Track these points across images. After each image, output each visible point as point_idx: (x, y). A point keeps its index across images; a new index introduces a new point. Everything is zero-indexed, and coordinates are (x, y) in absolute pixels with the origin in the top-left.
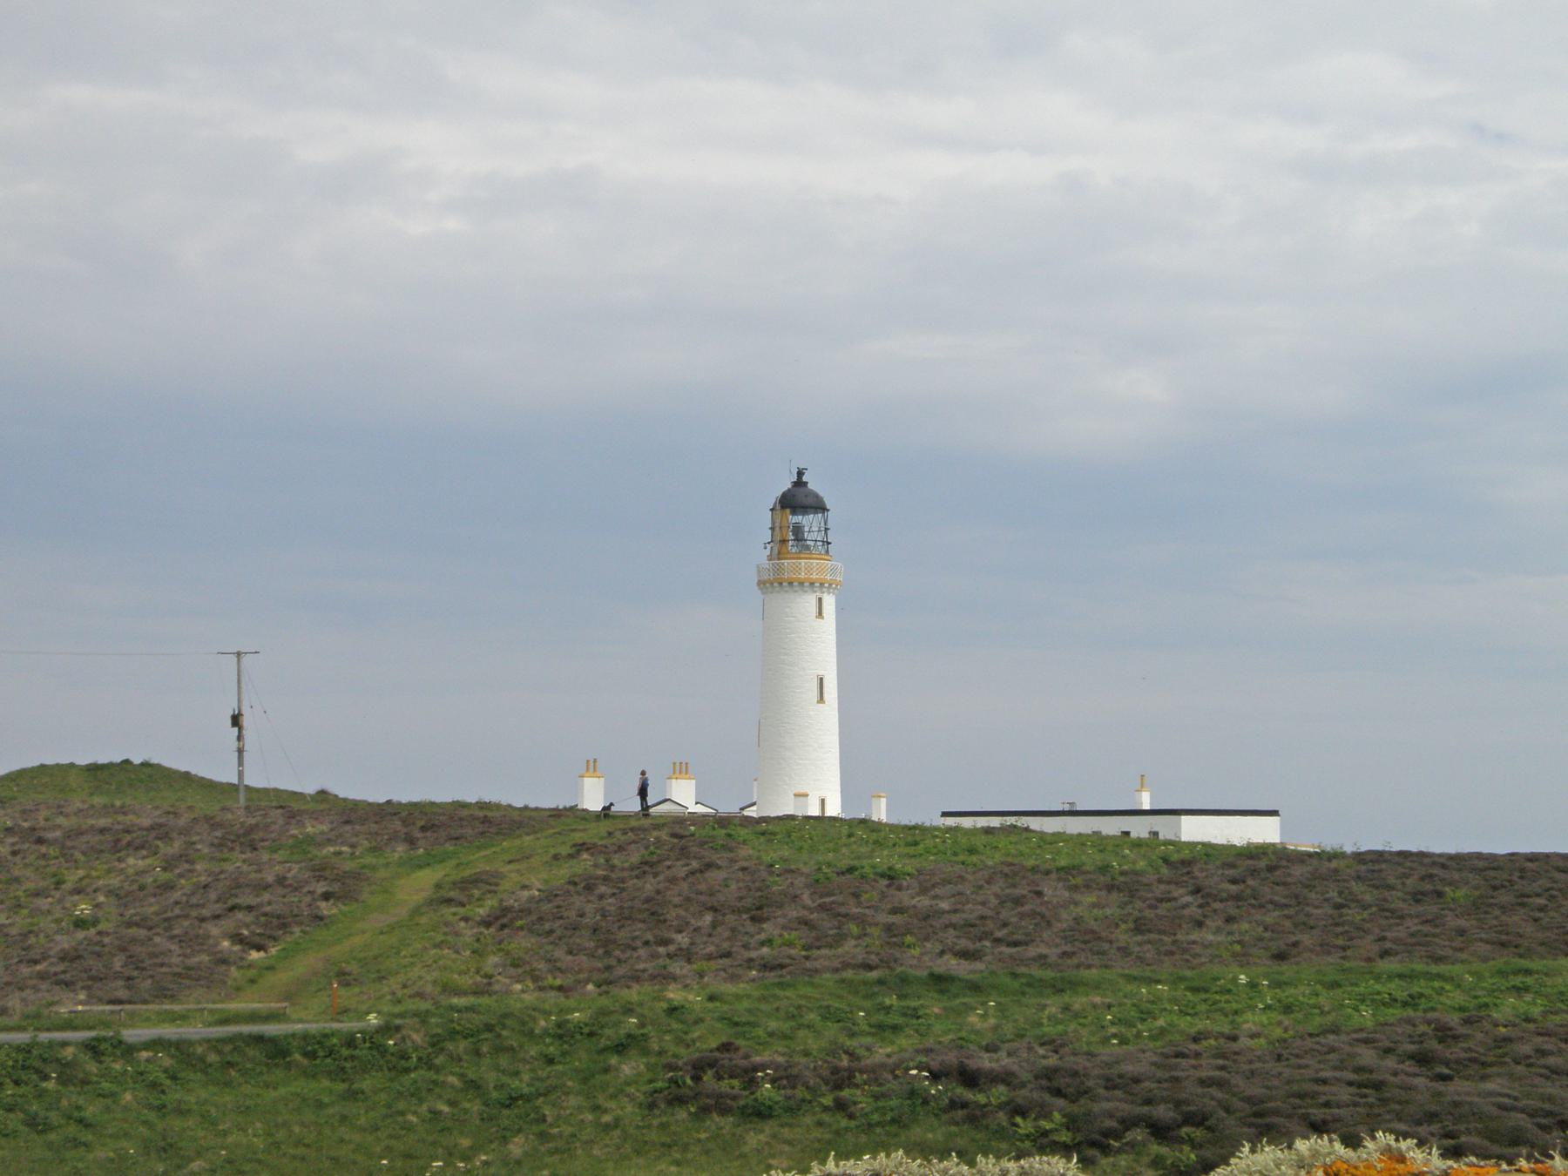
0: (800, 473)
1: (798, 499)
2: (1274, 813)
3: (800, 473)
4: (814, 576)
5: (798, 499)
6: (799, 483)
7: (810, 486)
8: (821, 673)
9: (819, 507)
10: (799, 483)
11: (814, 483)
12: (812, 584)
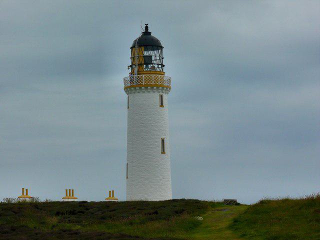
0: (147, 28)
1: (147, 42)
3: (147, 28)
4: (159, 84)
5: (147, 42)
6: (147, 33)
7: (152, 35)
8: (163, 137)
9: (156, 45)
10: (147, 33)
11: (155, 34)
12: (158, 88)
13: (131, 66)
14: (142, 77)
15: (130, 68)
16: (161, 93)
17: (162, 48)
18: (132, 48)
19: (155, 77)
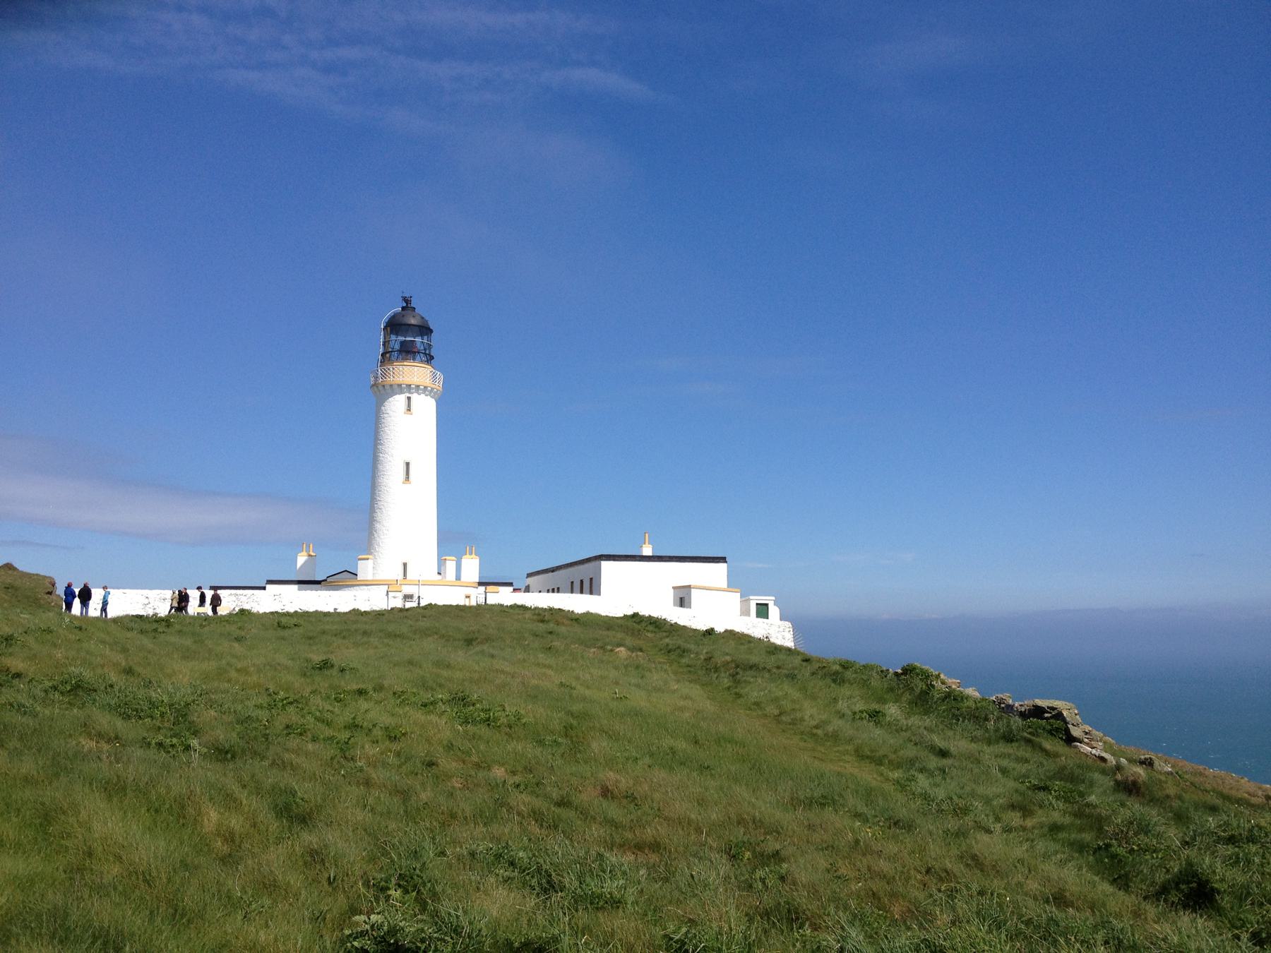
2: (722, 560)
9: (425, 330)
10: (408, 306)
11: (424, 310)
17: (431, 331)
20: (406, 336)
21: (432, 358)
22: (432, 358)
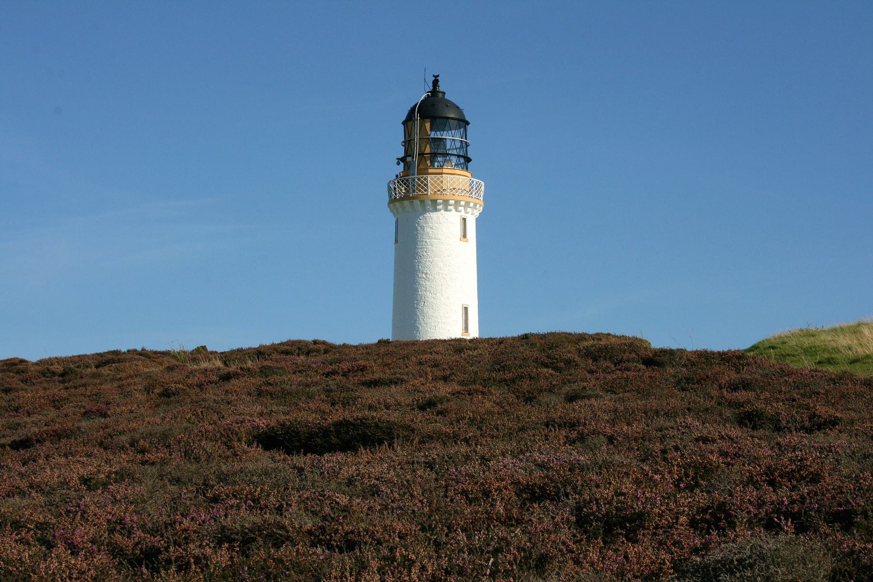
0: (436, 83)
3: (436, 83)
8: (466, 303)
9: (463, 123)
10: (435, 91)
11: (451, 91)
13: (403, 159)
14: (425, 179)
15: (402, 164)
16: (463, 214)
17: (467, 123)
18: (404, 123)
19: (451, 179)
20: (431, 127)
21: (468, 160)
22: (468, 160)
